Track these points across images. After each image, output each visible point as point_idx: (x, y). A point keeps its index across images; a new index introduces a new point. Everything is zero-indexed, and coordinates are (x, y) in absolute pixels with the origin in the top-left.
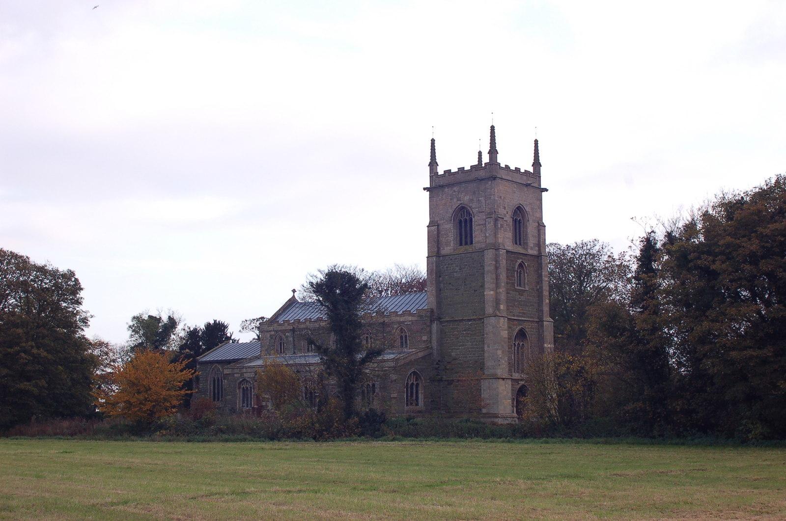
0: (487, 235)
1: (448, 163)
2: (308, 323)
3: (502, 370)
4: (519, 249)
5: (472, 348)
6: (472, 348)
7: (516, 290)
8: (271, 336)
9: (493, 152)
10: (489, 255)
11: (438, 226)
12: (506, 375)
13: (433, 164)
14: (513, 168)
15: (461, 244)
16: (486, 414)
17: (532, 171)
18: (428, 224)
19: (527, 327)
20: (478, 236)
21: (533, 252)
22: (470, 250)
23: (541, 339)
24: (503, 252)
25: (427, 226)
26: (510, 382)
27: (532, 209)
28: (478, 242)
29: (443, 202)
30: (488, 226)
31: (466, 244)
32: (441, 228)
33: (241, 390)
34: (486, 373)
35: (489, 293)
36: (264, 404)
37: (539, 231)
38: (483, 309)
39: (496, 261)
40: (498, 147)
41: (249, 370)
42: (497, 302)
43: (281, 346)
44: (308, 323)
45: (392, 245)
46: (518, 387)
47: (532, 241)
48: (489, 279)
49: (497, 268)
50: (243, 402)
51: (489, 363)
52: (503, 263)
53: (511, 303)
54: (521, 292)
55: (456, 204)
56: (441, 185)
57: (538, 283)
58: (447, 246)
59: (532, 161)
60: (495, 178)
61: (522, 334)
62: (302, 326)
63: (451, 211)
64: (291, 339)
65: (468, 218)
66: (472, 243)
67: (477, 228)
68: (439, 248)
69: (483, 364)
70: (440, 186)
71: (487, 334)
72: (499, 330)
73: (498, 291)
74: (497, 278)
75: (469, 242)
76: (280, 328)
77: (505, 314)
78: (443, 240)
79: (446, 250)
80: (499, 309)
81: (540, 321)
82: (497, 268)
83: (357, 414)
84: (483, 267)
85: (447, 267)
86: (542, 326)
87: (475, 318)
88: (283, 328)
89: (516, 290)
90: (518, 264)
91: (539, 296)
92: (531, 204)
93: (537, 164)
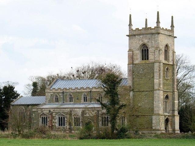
0: (155, 57)
1: (139, 24)
2: (70, 90)
3: (161, 112)
4: (166, 62)
5: (147, 103)
6: (147, 103)
7: (165, 79)
8: (51, 95)
9: (158, 22)
10: (156, 65)
11: (133, 51)
12: (162, 114)
13: (130, 25)
14: (165, 29)
15: (143, 59)
16: (155, 129)
17: (170, 29)
18: (128, 51)
19: (169, 94)
20: (151, 57)
21: (171, 63)
22: (147, 62)
23: (174, 99)
24: (162, 64)
25: (128, 52)
26: (163, 116)
27: (171, 45)
28: (151, 59)
29: (135, 42)
30: (156, 53)
31: (145, 59)
32: (134, 52)
33: (41, 118)
34: (154, 113)
35: (156, 81)
36: (54, 124)
37: (173, 54)
38: (153, 87)
39: (159, 68)
40: (160, 20)
41: (46, 110)
42: (160, 84)
43: (56, 99)
44: (70, 90)
45: (118, 59)
46: (166, 118)
47: (171, 59)
48: (156, 75)
49: (159, 70)
50: (42, 123)
51: (155, 109)
52: (162, 68)
53: (164, 84)
54: (167, 80)
55: (141, 43)
56: (133, 34)
57: (173, 76)
58: (137, 60)
59: (156, 21)
60: (159, 33)
61: (167, 97)
62: (68, 91)
63: (139, 46)
64: (62, 96)
65: (146, 49)
66: (148, 59)
67: (151, 53)
68: (133, 61)
69: (153, 109)
70: (134, 35)
71: (155, 97)
72: (160, 95)
73: (160, 80)
74: (160, 75)
75: (146, 58)
76: (56, 91)
77: (162, 89)
78: (135, 57)
79: (136, 62)
80: (160, 87)
81: (173, 92)
82: (159, 70)
83: (117, 130)
84: (153, 70)
85: (137, 69)
86: (174, 94)
87: (150, 90)
88: (58, 91)
89: (165, 79)
90: (166, 68)
91: (173, 81)
92: (170, 43)
93: (172, 26)
